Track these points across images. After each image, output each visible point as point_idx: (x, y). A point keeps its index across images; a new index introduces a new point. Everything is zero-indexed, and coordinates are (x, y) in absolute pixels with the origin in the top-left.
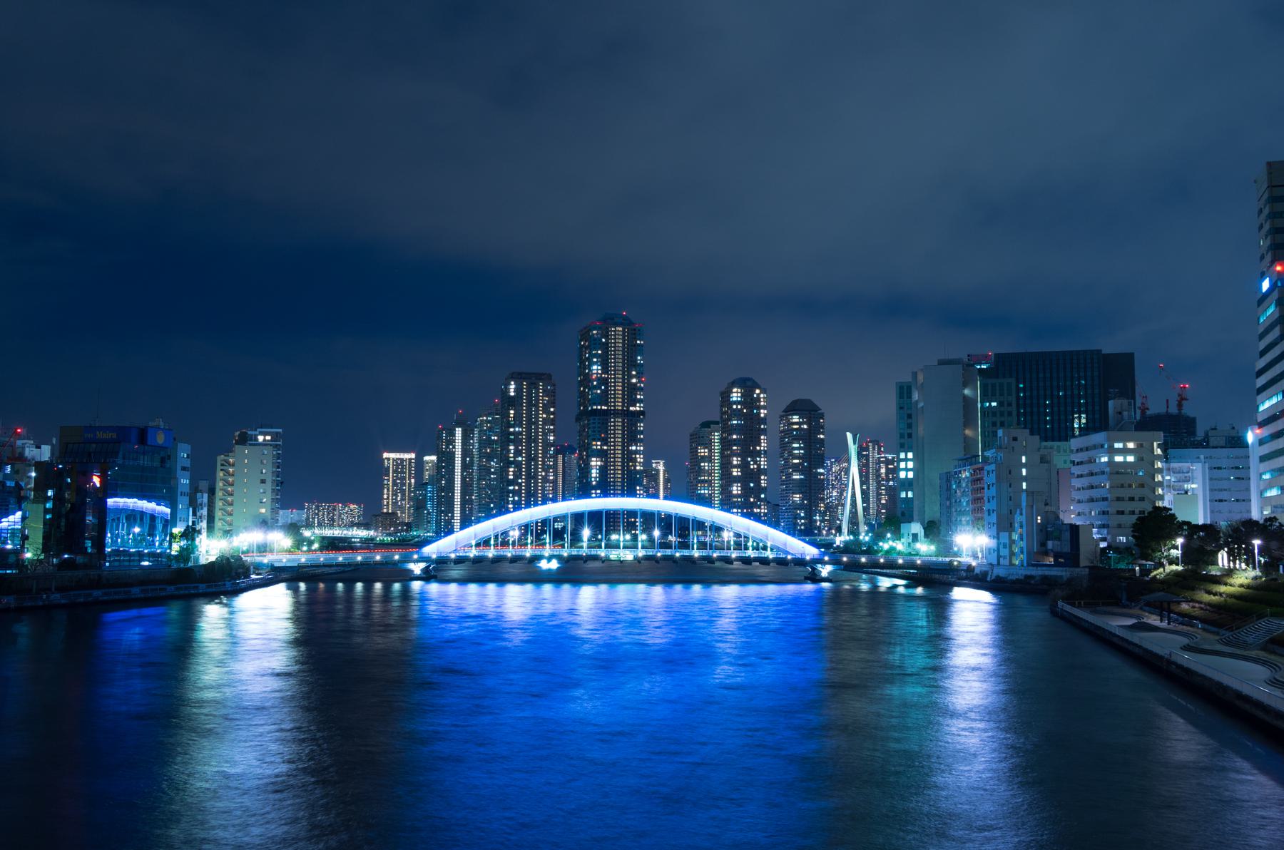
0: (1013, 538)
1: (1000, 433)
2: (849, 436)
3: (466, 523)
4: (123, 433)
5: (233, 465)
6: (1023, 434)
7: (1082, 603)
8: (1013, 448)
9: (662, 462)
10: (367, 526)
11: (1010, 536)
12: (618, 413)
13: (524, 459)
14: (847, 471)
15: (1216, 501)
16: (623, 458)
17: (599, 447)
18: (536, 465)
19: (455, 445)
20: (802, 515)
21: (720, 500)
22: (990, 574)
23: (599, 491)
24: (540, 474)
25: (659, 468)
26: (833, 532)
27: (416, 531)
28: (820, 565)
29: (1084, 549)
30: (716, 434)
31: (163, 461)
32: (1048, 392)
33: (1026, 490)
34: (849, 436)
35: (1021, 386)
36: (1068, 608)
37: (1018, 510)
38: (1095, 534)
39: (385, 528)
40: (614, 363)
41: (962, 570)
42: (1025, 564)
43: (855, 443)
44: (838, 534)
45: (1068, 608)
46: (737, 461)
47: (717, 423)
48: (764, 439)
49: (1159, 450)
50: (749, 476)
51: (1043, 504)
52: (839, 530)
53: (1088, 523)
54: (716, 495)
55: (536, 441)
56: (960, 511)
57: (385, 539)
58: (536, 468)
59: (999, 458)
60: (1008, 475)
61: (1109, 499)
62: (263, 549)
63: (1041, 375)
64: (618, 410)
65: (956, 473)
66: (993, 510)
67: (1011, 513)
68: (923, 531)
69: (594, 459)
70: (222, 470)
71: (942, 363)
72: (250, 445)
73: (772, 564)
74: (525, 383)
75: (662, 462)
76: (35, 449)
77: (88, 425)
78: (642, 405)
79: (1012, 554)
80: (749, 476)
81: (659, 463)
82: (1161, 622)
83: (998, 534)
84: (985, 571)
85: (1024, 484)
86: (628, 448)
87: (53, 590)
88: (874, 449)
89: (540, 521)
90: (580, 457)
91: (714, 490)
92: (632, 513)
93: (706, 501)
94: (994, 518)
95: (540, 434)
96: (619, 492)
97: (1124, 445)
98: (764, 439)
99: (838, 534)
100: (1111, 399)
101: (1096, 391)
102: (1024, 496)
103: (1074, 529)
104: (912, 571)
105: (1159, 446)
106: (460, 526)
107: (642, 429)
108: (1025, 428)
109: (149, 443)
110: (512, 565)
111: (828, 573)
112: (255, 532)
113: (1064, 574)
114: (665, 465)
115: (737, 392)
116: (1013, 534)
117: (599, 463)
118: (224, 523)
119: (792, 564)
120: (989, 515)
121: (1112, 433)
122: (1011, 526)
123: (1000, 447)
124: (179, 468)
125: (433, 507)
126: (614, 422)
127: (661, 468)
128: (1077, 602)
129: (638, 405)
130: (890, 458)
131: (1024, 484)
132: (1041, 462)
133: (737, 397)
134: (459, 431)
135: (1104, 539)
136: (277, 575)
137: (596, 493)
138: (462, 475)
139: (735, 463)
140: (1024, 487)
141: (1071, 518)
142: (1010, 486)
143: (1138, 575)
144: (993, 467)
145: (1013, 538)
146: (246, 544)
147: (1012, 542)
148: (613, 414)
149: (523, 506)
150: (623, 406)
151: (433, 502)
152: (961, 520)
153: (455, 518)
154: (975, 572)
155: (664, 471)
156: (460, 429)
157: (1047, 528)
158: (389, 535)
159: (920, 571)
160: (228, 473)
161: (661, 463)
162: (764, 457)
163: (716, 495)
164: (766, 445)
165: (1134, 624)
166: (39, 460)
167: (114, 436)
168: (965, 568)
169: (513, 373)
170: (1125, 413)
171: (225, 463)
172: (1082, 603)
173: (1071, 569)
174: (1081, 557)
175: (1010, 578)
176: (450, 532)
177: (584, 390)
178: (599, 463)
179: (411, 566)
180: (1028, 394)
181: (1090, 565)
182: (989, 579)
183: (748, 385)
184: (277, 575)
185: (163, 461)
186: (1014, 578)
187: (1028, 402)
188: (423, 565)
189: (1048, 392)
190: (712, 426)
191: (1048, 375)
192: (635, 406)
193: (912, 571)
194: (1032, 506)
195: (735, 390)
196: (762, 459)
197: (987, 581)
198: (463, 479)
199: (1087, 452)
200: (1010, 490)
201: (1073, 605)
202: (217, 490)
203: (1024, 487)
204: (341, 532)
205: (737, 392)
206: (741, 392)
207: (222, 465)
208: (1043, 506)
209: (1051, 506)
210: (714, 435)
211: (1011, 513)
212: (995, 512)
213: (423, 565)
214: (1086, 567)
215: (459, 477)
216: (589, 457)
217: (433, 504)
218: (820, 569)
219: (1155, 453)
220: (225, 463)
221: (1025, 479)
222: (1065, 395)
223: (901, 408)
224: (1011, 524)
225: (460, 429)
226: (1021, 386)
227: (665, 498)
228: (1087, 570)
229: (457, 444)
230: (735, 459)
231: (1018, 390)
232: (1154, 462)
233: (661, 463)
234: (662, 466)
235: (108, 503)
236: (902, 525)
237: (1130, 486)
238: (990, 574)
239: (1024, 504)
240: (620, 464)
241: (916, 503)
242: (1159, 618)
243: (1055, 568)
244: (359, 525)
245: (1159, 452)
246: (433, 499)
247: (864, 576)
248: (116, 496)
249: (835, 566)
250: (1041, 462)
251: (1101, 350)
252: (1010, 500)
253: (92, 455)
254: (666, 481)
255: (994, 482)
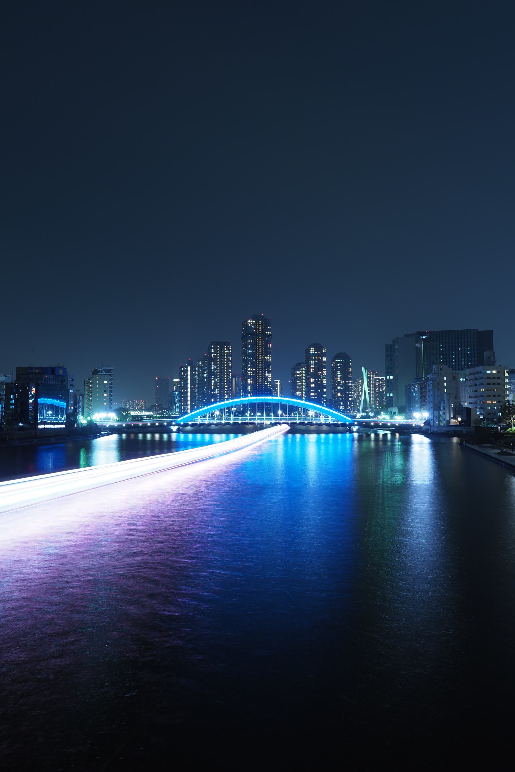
0: (440, 414)
1: (434, 367)
2: (363, 368)
3: (193, 408)
4: (45, 370)
5: (92, 384)
6: (445, 367)
7: (474, 442)
8: (440, 373)
9: (279, 381)
10: (149, 410)
11: (439, 413)
12: (260, 335)
13: (218, 380)
14: (362, 385)
15: (179, 436)
16: (262, 379)
17: (251, 375)
18: (224, 383)
19: (187, 374)
20: (342, 404)
21: (305, 398)
22: (430, 430)
23: (252, 394)
24: (225, 386)
25: (278, 383)
26: (356, 411)
27: (171, 412)
28: (353, 426)
29: (473, 417)
30: (303, 368)
31: (62, 382)
32: (454, 349)
33: (446, 392)
34: (363, 368)
35: (441, 346)
36: (468, 445)
37: (443, 401)
38: (478, 412)
39: (157, 411)
40: (258, 363)
41: (417, 428)
42: (446, 425)
43: (365, 372)
44: (358, 413)
45: (468, 445)
46: (313, 380)
47: (303, 363)
48: (325, 371)
49: (507, 374)
50: (319, 386)
51: (454, 398)
52: (358, 411)
53: (474, 407)
54: (303, 396)
55: (223, 372)
56: (415, 402)
57: (157, 416)
58: (224, 384)
59: (434, 378)
60: (439, 386)
61: (484, 396)
62: (107, 419)
63: (450, 341)
64: (260, 333)
65: (413, 385)
66: (431, 401)
67: (439, 403)
68: (398, 411)
69: (249, 380)
70: (87, 386)
71: (406, 335)
72: (99, 374)
73: (331, 426)
74: (218, 346)
75: (279, 381)
76: (4, 377)
77: (29, 367)
78: (270, 356)
79: (440, 421)
80: (319, 386)
81: (277, 381)
82: (513, 451)
83: (433, 412)
84: (427, 429)
85: (445, 390)
86: (264, 357)
87: (16, 439)
88: (373, 375)
89: (218, 402)
90: (243, 379)
91: (303, 393)
92: (268, 404)
93: (300, 398)
94: (431, 405)
95: (225, 369)
96: (261, 393)
97: (491, 372)
98: (325, 371)
99: (358, 413)
100: (485, 351)
101: (476, 348)
102: (445, 395)
103: (468, 410)
104: (394, 429)
105: (507, 372)
106: (190, 411)
107: (270, 361)
108: (446, 364)
109: (56, 374)
110: (334, 427)
111: (357, 430)
112: (112, 413)
113: (463, 430)
114: (280, 382)
115: (313, 350)
116: (440, 412)
117: (252, 382)
118: (88, 409)
119: (340, 426)
120: (429, 403)
121: (486, 367)
122: (439, 409)
123: (435, 373)
124: (69, 385)
125: (178, 402)
126: (258, 339)
127: (278, 384)
128: (472, 442)
129: (269, 356)
130: (380, 378)
131: (445, 390)
132: (453, 380)
133: (313, 352)
134: (189, 368)
135: (481, 414)
136: (112, 430)
137: (250, 395)
138: (191, 387)
139: (312, 381)
140: (445, 391)
141: (466, 405)
142: (439, 391)
143: (499, 430)
144: (431, 382)
145: (440, 414)
146: (99, 418)
147: (440, 416)
148: (257, 335)
149: (218, 401)
150: (262, 332)
151: (178, 399)
152: (415, 406)
153: (188, 405)
154: (423, 429)
155: (280, 385)
156: (190, 367)
157: (456, 409)
158: (158, 414)
159: (397, 429)
160: (90, 387)
161: (279, 381)
162: (325, 379)
163: (303, 396)
164: (325, 373)
165: (500, 452)
166: (6, 382)
167: (41, 371)
168: (418, 427)
169: (213, 342)
170: (492, 358)
171: (88, 383)
172: (474, 442)
173: (467, 428)
174: (471, 422)
175: (439, 431)
176: (186, 413)
177: (245, 349)
178: (252, 382)
179: (172, 428)
180: (444, 349)
181: (475, 426)
182: (429, 432)
183: (318, 348)
184: (112, 430)
185: (62, 382)
186: (441, 432)
187: (444, 353)
188: (177, 427)
189: (454, 349)
190: (301, 365)
191: (450, 341)
192: (268, 356)
193: (394, 429)
194: (449, 399)
195: (312, 349)
196: (324, 379)
197: (428, 433)
198: (191, 389)
199: (473, 375)
200: (439, 392)
201: (470, 444)
202: (85, 395)
203: (445, 391)
204: (137, 413)
205: (313, 350)
206: (314, 350)
207: (87, 384)
208: (454, 400)
209: (457, 399)
210: (302, 369)
211: (439, 403)
212: (432, 402)
213: (177, 427)
214: (474, 427)
215: (190, 388)
216: (247, 379)
217: (178, 400)
218: (353, 428)
219: (505, 376)
220: (88, 383)
221: (446, 387)
222: (461, 350)
223: (388, 356)
224: (439, 407)
225: (190, 367)
226: (441, 346)
227: (280, 396)
228: (474, 428)
229: (188, 374)
230: (312, 379)
231: (440, 347)
232: (505, 379)
233: (279, 381)
234: (279, 382)
235: (39, 401)
236: (388, 408)
237: (494, 390)
238: (430, 430)
239: (445, 399)
240: (261, 380)
241: (394, 399)
242: (512, 450)
243: (460, 427)
244: (145, 410)
245: (507, 375)
246: (178, 397)
247: (372, 430)
248: (42, 397)
249: (360, 427)
250: (453, 380)
251: (478, 329)
252: (439, 397)
253: (31, 379)
254: (281, 389)
255: (432, 389)
